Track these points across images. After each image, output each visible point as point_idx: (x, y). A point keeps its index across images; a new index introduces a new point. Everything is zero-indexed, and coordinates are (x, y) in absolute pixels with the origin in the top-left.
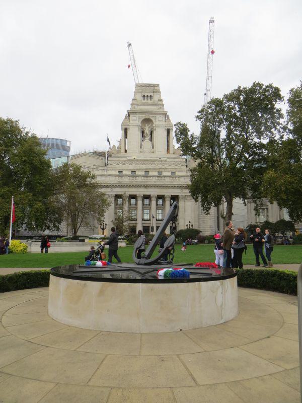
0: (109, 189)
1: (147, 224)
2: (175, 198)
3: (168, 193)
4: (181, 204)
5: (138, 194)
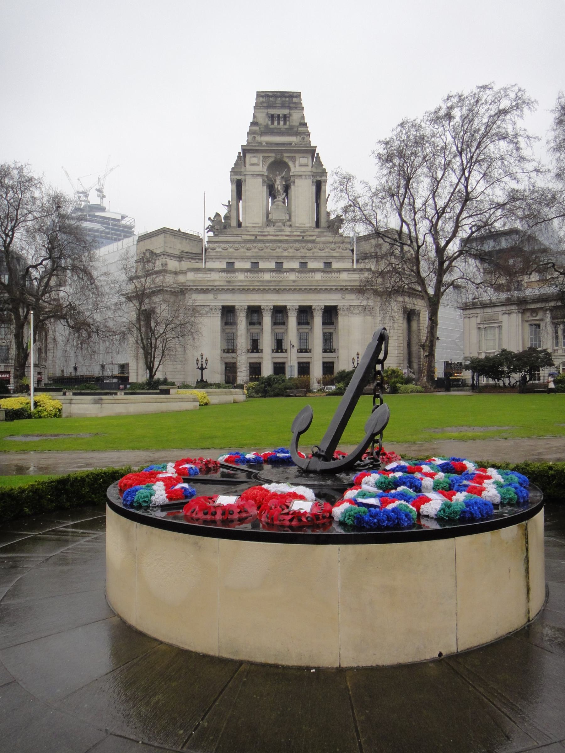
0: (211, 296)
1: (280, 358)
2: (330, 314)
3: (319, 301)
4: (342, 320)
5: (263, 304)
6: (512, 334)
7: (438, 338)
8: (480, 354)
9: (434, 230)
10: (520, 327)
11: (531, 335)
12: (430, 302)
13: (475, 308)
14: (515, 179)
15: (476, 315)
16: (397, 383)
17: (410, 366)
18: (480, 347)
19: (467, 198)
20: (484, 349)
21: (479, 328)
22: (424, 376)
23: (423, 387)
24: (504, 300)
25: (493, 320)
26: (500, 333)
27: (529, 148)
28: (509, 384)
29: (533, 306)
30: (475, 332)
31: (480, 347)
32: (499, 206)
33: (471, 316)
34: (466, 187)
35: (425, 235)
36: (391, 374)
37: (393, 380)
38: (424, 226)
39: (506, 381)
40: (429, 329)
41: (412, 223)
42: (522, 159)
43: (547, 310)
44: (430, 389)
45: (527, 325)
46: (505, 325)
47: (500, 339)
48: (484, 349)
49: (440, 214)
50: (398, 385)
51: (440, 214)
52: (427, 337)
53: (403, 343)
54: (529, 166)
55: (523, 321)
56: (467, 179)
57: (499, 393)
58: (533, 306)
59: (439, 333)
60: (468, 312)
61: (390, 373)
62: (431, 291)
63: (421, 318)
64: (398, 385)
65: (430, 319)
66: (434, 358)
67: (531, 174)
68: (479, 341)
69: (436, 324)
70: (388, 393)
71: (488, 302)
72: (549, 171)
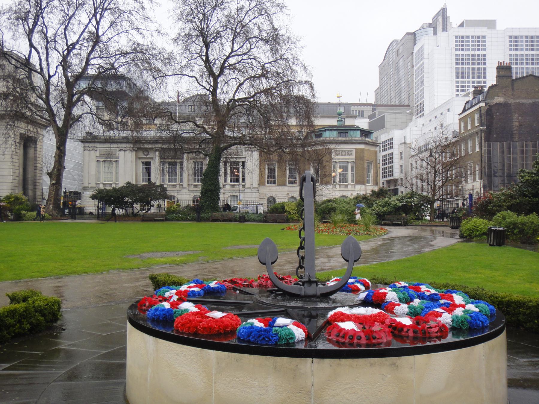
6: (126, 170)
7: (65, 169)
8: (98, 184)
9: (65, 64)
10: (134, 163)
11: (143, 170)
12: (58, 132)
13: (94, 142)
14: (141, 34)
15: (95, 149)
16: (22, 210)
17: (25, 193)
18: (98, 179)
19: (96, 39)
20: (102, 180)
21: (98, 161)
22: (50, 204)
23: (50, 215)
24: (121, 138)
25: (112, 154)
26: (117, 167)
27: (152, 11)
28: (133, 213)
29: (146, 146)
30: (94, 164)
31: (98, 179)
32: (125, 54)
33: (91, 149)
34: (97, 30)
35: (57, 67)
36: (14, 201)
37: (17, 207)
38: (55, 58)
39: (130, 210)
40: (57, 158)
41: (42, 51)
42: (146, 18)
43: (156, 150)
44: (57, 216)
45: (140, 162)
46: (121, 160)
47: (117, 173)
48: (102, 180)
49: (71, 48)
50: (23, 212)
51: (71, 48)
52: (55, 166)
53: (19, 170)
54: (153, 27)
55: (138, 158)
56: (98, 23)
57: (124, 221)
58: (146, 146)
59: (66, 164)
60: (87, 145)
61: (13, 199)
62: (60, 124)
63: (38, 146)
64: (23, 212)
65: (58, 148)
66: (61, 187)
67: (153, 33)
68: (98, 172)
69: (64, 154)
70: (12, 220)
71: (108, 137)
72: (167, 35)
